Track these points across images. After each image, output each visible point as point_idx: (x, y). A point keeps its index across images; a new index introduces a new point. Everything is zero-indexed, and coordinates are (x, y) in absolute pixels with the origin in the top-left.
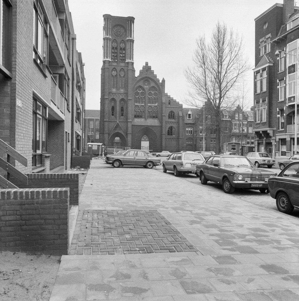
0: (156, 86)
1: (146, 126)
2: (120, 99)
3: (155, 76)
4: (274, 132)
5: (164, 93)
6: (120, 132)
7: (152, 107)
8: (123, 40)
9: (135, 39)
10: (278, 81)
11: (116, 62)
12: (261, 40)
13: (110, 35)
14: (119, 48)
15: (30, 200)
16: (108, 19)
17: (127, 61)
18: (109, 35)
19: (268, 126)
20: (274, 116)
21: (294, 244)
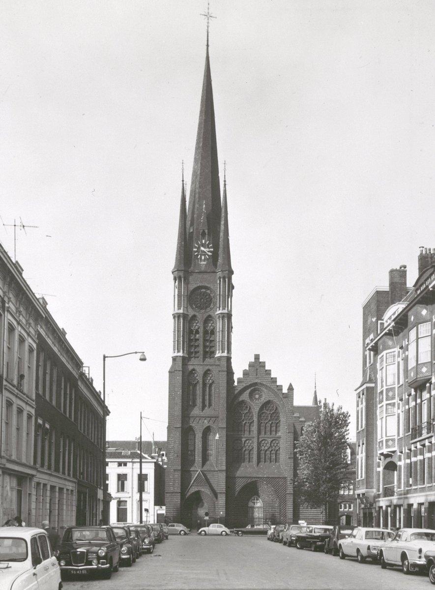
3: (274, 380)
15: (374, 469)
21: (79, 383)
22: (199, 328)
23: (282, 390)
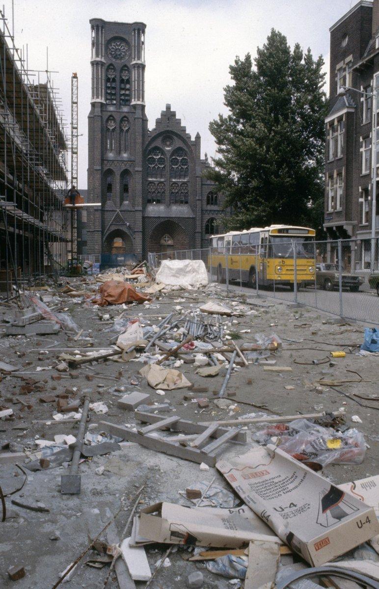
0: (185, 148)
1: (166, 219)
2: (122, 170)
3: (184, 129)
4: (354, 228)
5: (200, 158)
6: (121, 228)
7: (155, 184)
8: (125, 66)
9: (146, 64)
10: (361, 140)
11: (114, 104)
12: (338, 67)
13: (102, 56)
14: (118, 79)
16: (97, 26)
17: (133, 102)
18: (100, 56)
19: (344, 218)
20: (354, 200)
22: (115, 77)
23: (180, 123)
